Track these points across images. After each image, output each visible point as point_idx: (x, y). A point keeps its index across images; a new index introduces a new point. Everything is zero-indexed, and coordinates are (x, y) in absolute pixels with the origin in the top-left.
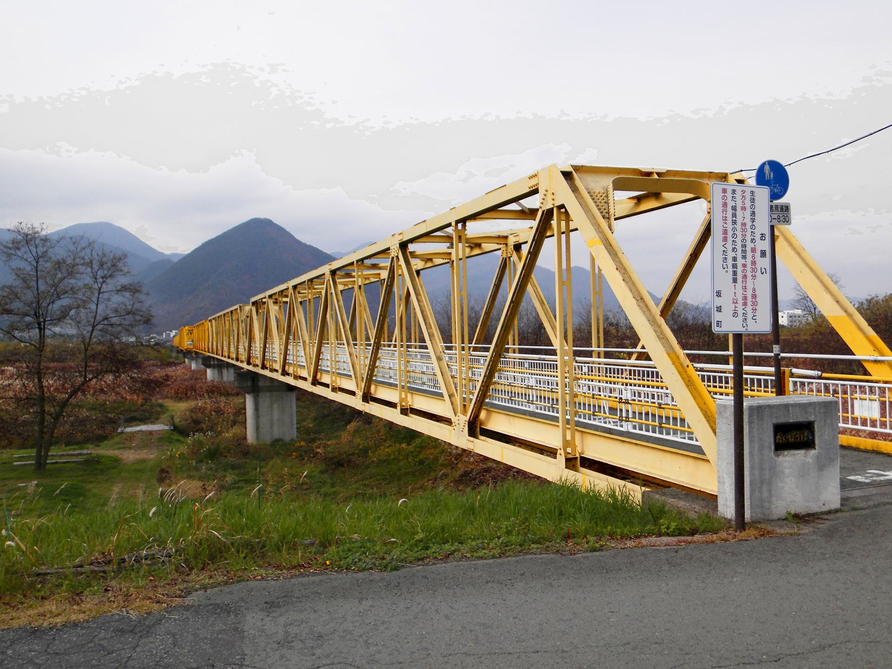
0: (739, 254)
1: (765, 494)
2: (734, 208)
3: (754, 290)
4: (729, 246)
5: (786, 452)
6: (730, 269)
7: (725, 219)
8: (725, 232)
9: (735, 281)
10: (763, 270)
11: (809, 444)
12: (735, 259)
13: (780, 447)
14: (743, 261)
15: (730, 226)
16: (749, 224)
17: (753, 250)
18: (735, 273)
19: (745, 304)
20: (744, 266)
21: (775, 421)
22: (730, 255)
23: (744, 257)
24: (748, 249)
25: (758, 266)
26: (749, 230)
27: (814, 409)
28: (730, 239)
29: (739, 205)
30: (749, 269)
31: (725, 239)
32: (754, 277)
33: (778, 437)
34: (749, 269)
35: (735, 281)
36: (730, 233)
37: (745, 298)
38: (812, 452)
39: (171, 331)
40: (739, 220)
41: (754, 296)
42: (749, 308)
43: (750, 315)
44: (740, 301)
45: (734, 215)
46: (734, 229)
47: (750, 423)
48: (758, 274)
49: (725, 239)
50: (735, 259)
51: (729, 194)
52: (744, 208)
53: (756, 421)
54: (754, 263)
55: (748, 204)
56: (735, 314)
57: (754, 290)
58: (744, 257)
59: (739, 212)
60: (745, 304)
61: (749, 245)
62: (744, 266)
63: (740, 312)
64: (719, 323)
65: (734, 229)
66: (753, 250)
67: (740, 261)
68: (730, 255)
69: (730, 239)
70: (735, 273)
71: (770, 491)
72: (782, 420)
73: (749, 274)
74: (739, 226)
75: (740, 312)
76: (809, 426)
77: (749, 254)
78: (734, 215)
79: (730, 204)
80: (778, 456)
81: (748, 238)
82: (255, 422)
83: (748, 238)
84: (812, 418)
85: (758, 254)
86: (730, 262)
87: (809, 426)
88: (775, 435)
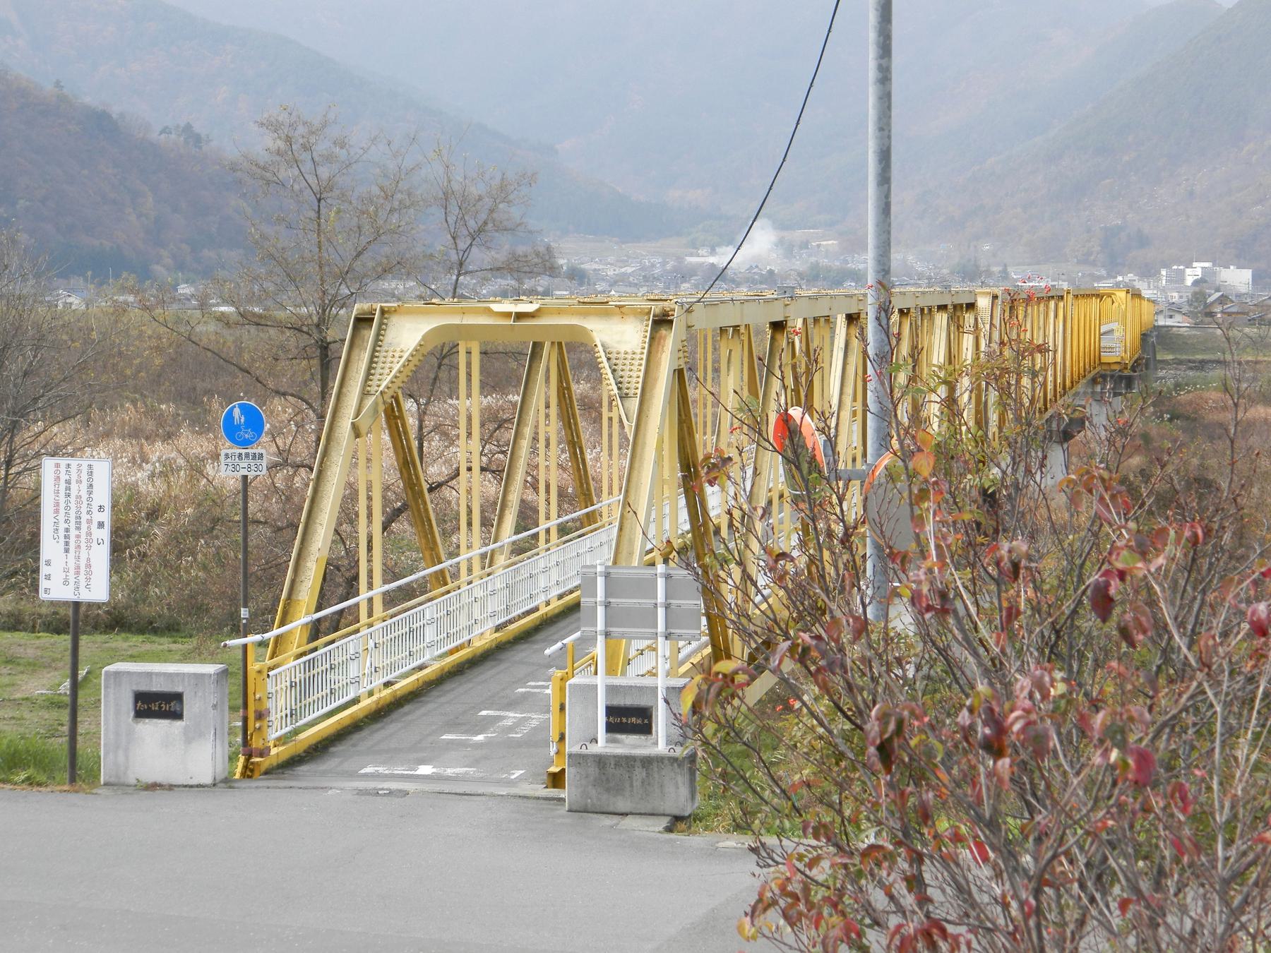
0: (73, 525)
1: (121, 758)
2: (68, 482)
3: (88, 560)
4: (61, 517)
5: (147, 720)
6: (62, 540)
7: (57, 492)
8: (57, 504)
9: (67, 551)
10: (100, 541)
11: (178, 716)
12: (67, 530)
13: (140, 714)
14: (77, 533)
15: (62, 499)
16: (85, 496)
17: (89, 522)
18: (67, 544)
19: (78, 573)
20: (78, 536)
21: (135, 688)
22: (62, 526)
23: (78, 528)
24: (83, 521)
25: (94, 537)
26: (85, 503)
27: (183, 680)
28: (62, 511)
29: (74, 478)
30: (83, 539)
31: (57, 511)
32: (89, 548)
33: (139, 704)
34: (83, 539)
35: (67, 551)
36: (62, 505)
37: (78, 567)
38: (178, 723)
39: (1189, 266)
40: (74, 492)
41: (89, 566)
42: (82, 577)
43: (83, 583)
44: (72, 571)
45: (68, 489)
46: (67, 502)
47: (106, 687)
48: (94, 544)
49: (57, 511)
50: (67, 530)
51: (63, 469)
52: (79, 482)
53: (112, 686)
54: (89, 534)
55: (84, 477)
56: (66, 582)
57: (88, 560)
58: (78, 528)
59: (74, 486)
60: (78, 573)
61: (85, 517)
62: (78, 536)
63: (72, 580)
64: (46, 590)
65: (67, 502)
66: (89, 522)
67: (73, 533)
68: (62, 526)
69: (62, 511)
70: (67, 544)
71: (127, 757)
72: (144, 688)
73: (83, 545)
74: (73, 499)
75: (72, 580)
76: (178, 697)
77: (84, 526)
78: (68, 489)
79: (63, 477)
80: (137, 723)
81: (84, 509)
82: (388, 701)
83: (84, 509)
84: (179, 689)
85: (95, 525)
86: (62, 533)
87: (178, 697)
88: (136, 702)
